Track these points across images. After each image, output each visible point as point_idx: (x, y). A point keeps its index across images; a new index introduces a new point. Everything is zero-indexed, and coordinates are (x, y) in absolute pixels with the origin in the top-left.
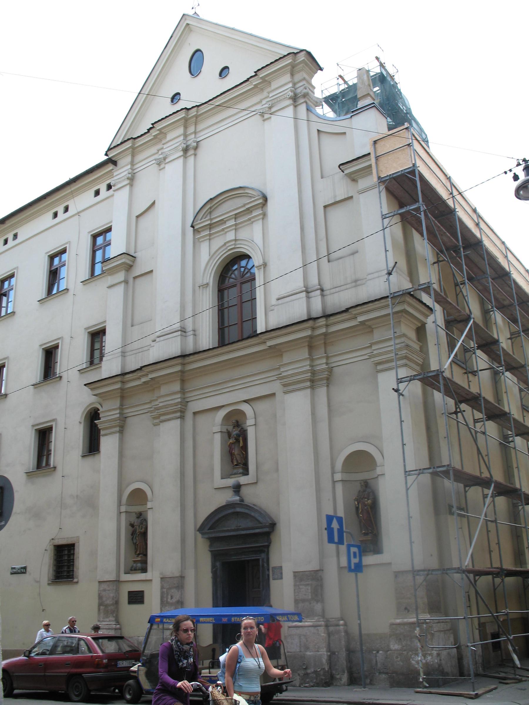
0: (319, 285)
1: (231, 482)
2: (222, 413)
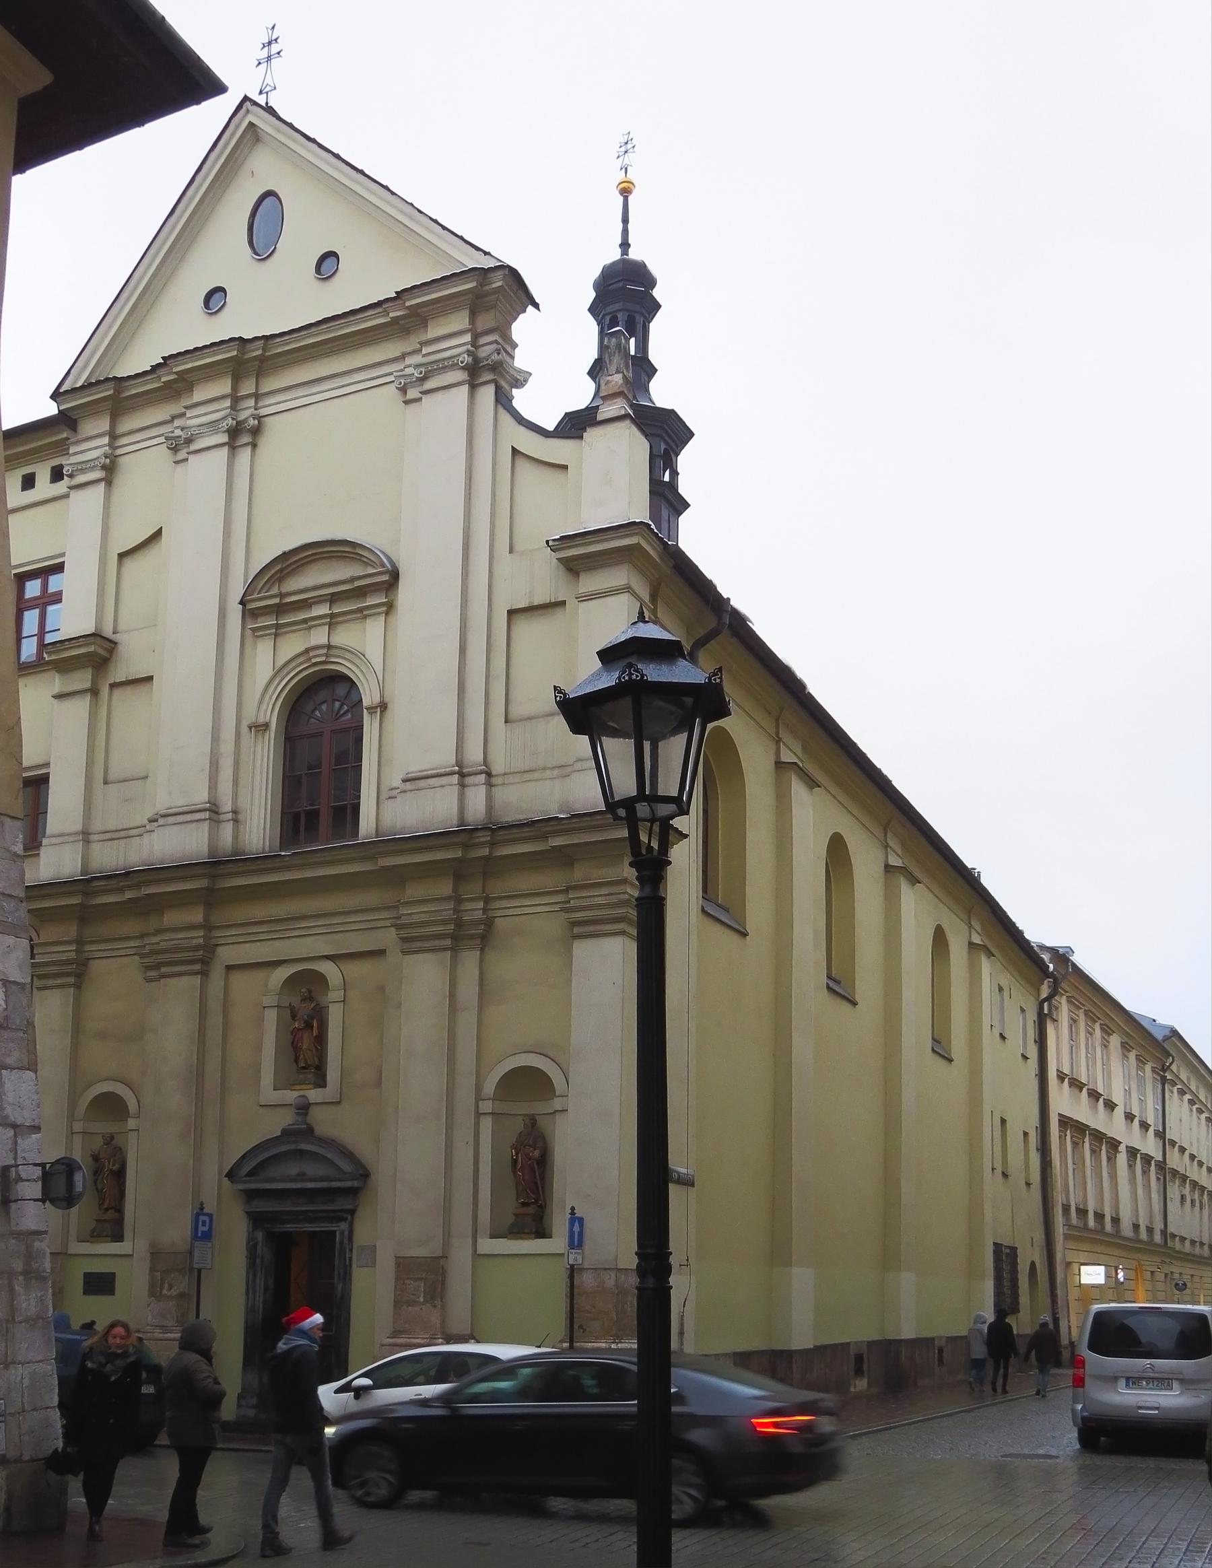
0: (485, 763)
1: (291, 1096)
2: (282, 973)
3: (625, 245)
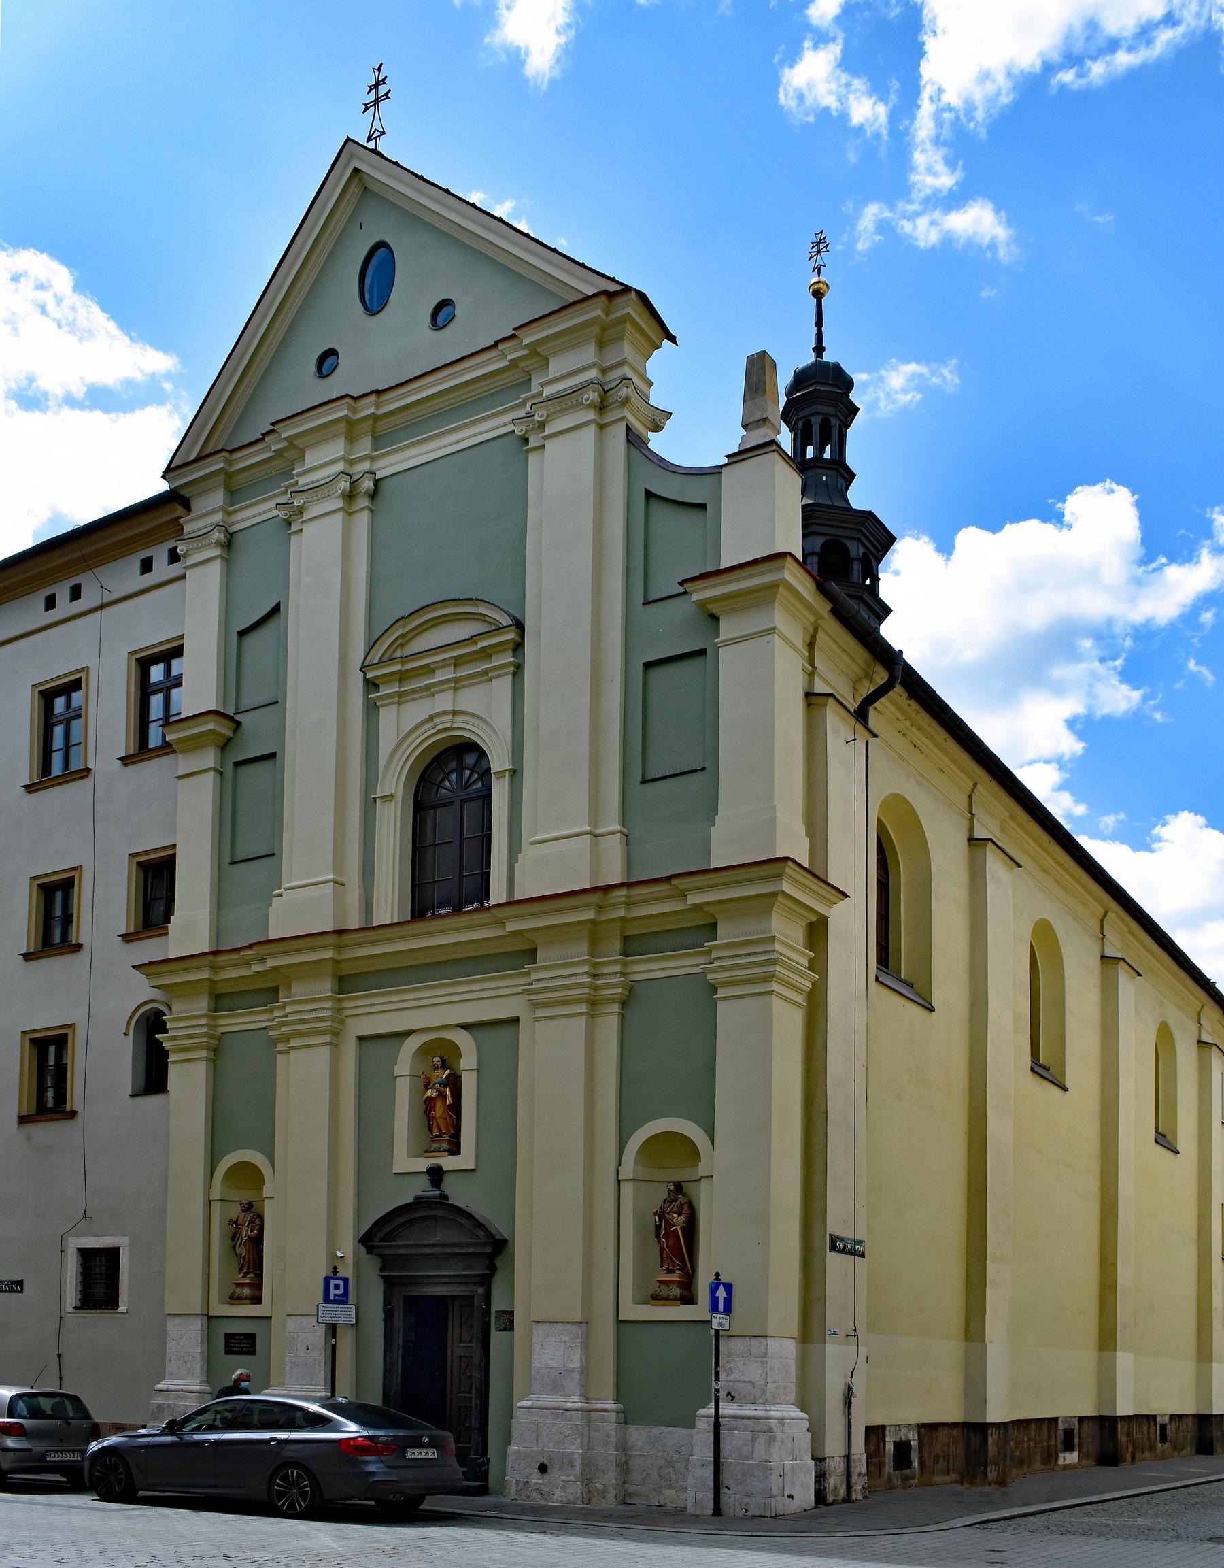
2: (411, 1046)
3: (819, 349)
